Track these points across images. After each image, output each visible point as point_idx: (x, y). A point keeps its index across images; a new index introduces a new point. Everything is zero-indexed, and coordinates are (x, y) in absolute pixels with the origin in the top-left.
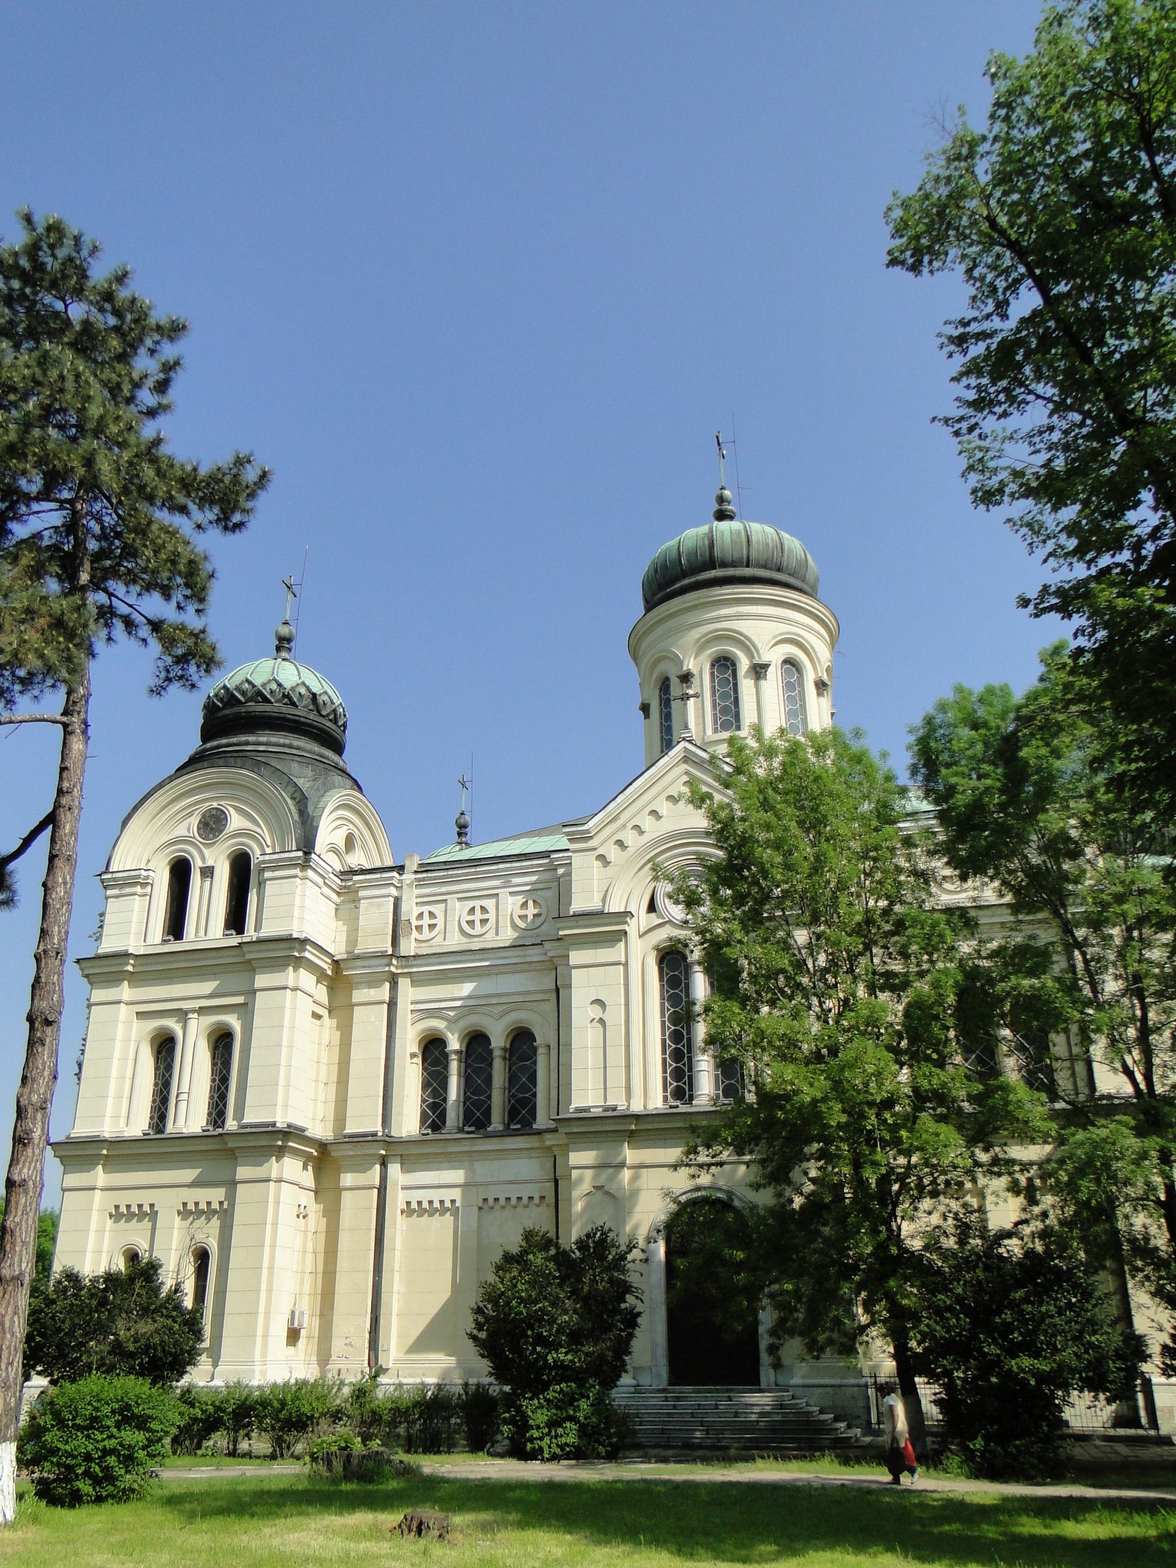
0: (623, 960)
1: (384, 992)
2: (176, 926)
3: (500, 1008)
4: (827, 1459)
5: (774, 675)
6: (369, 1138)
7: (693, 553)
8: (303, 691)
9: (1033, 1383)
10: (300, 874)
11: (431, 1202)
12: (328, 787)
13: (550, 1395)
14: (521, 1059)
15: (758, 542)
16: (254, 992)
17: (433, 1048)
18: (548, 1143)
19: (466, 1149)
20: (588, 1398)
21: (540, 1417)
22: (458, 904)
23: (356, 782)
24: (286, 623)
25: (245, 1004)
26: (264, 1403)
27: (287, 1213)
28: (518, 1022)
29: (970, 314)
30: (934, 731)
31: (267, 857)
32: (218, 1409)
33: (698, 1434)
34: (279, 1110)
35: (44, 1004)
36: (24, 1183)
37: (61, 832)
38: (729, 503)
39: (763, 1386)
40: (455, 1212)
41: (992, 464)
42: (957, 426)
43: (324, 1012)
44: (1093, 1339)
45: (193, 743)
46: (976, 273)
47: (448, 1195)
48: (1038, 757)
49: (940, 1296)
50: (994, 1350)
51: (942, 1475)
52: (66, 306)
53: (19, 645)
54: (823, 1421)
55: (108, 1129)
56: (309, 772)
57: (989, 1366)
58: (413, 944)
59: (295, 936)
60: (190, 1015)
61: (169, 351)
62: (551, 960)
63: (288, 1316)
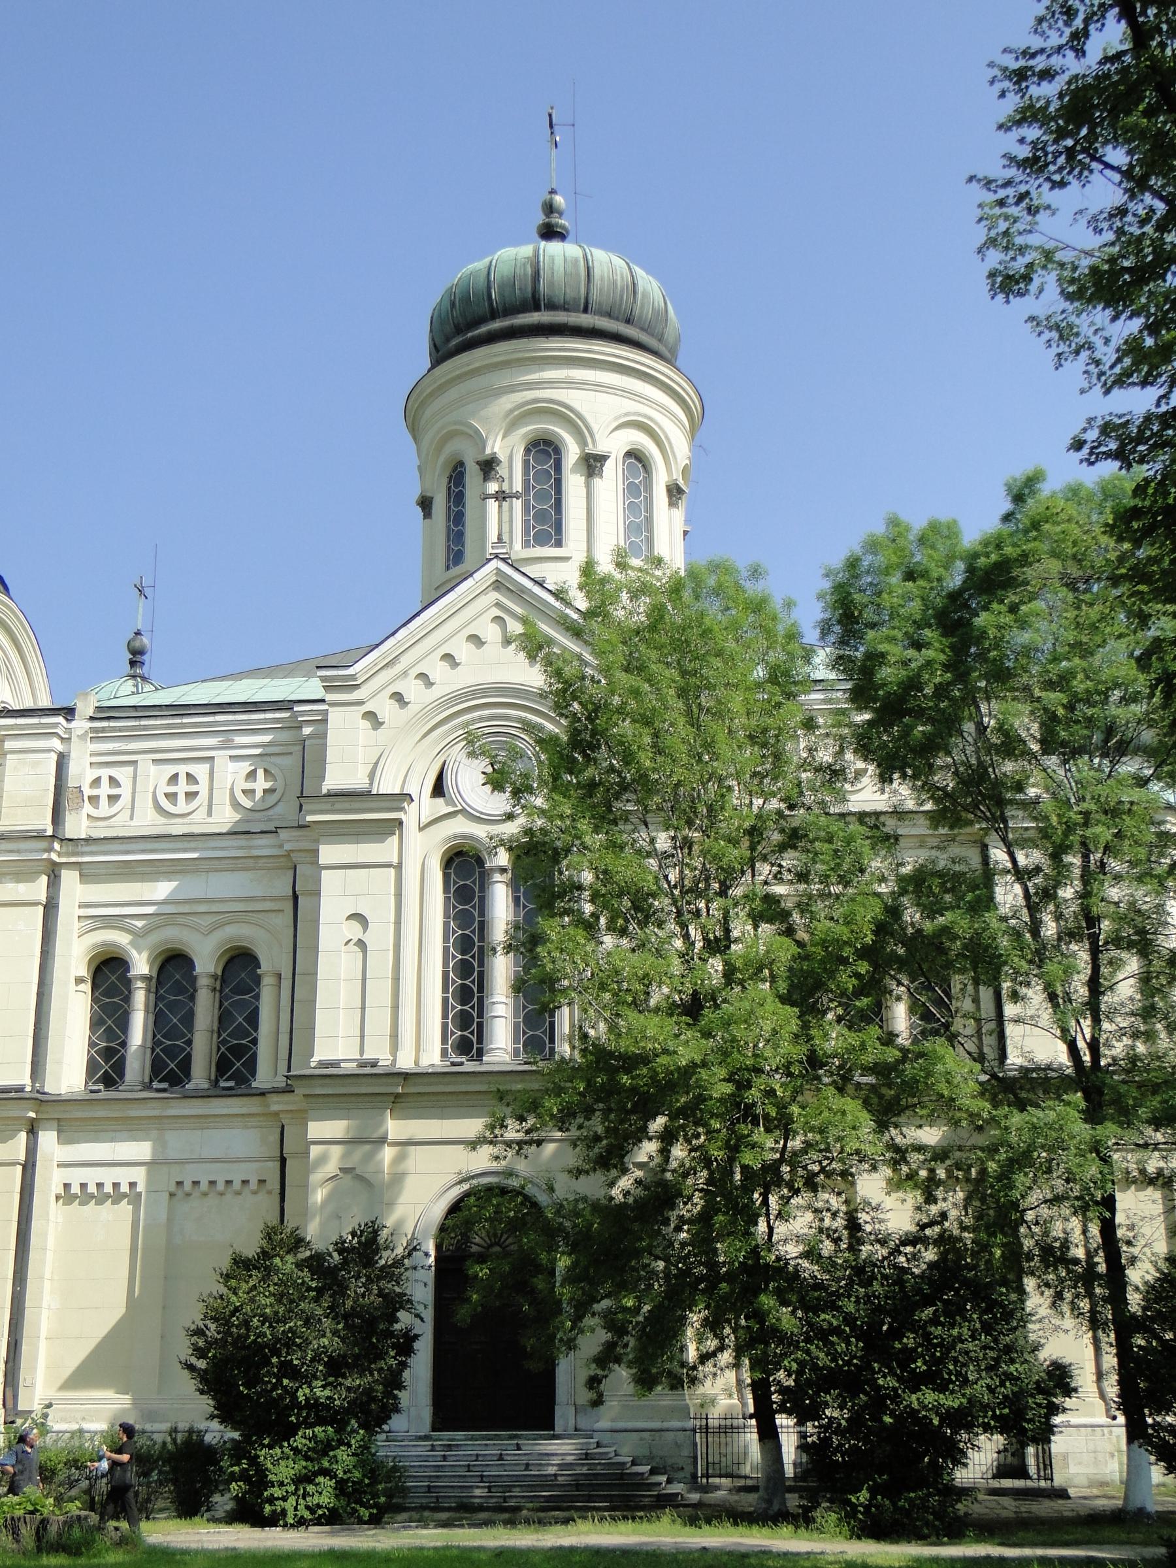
0: (395, 861)
1: (39, 889)
3: (206, 921)
4: (666, 1519)
5: (613, 473)
6: (12, 1095)
7: (510, 283)
9: (936, 1422)
13: (299, 1441)
15: (602, 278)
18: (275, 1108)
20: (350, 1446)
22: (153, 769)
29: (1036, 43)
30: (857, 577)
38: (561, 214)
39: (558, 1429)
40: (133, 1197)
41: (1019, 240)
42: (1002, 193)
44: (1012, 1368)
47: (124, 1176)
48: (1000, 628)
49: (823, 1316)
50: (892, 1382)
51: (815, 1535)
54: (637, 1474)
58: (85, 822)
62: (288, 855)
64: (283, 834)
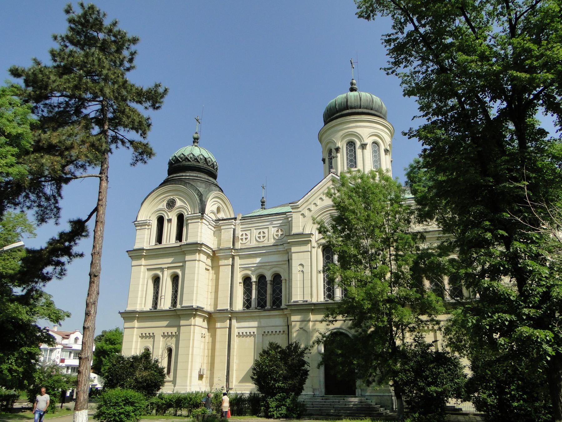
1: (230, 261)
2: (159, 240)
3: (269, 267)
5: (369, 148)
7: (340, 104)
8: (202, 157)
9: (435, 395)
10: (200, 221)
11: (246, 333)
12: (210, 191)
13: (277, 397)
14: (277, 284)
15: (364, 100)
16: (185, 262)
17: (247, 280)
18: (285, 313)
19: (258, 315)
20: (290, 398)
21: (273, 404)
23: (220, 189)
24: (196, 133)
25: (182, 266)
26: (185, 399)
27: (198, 336)
28: (275, 271)
31: (189, 215)
32: (170, 400)
33: (332, 411)
34: (194, 302)
35: (94, 270)
36: (88, 328)
37: (99, 213)
38: (355, 85)
40: (254, 336)
43: (210, 268)
45: (165, 176)
46: (395, 17)
47: (252, 330)
50: (422, 384)
52: (98, 34)
53: (79, 153)
55: (138, 308)
56: (204, 185)
57: (421, 389)
58: (240, 245)
59: (199, 242)
60: (165, 270)
61: (133, 48)
63: (198, 370)
64: (285, 245)
